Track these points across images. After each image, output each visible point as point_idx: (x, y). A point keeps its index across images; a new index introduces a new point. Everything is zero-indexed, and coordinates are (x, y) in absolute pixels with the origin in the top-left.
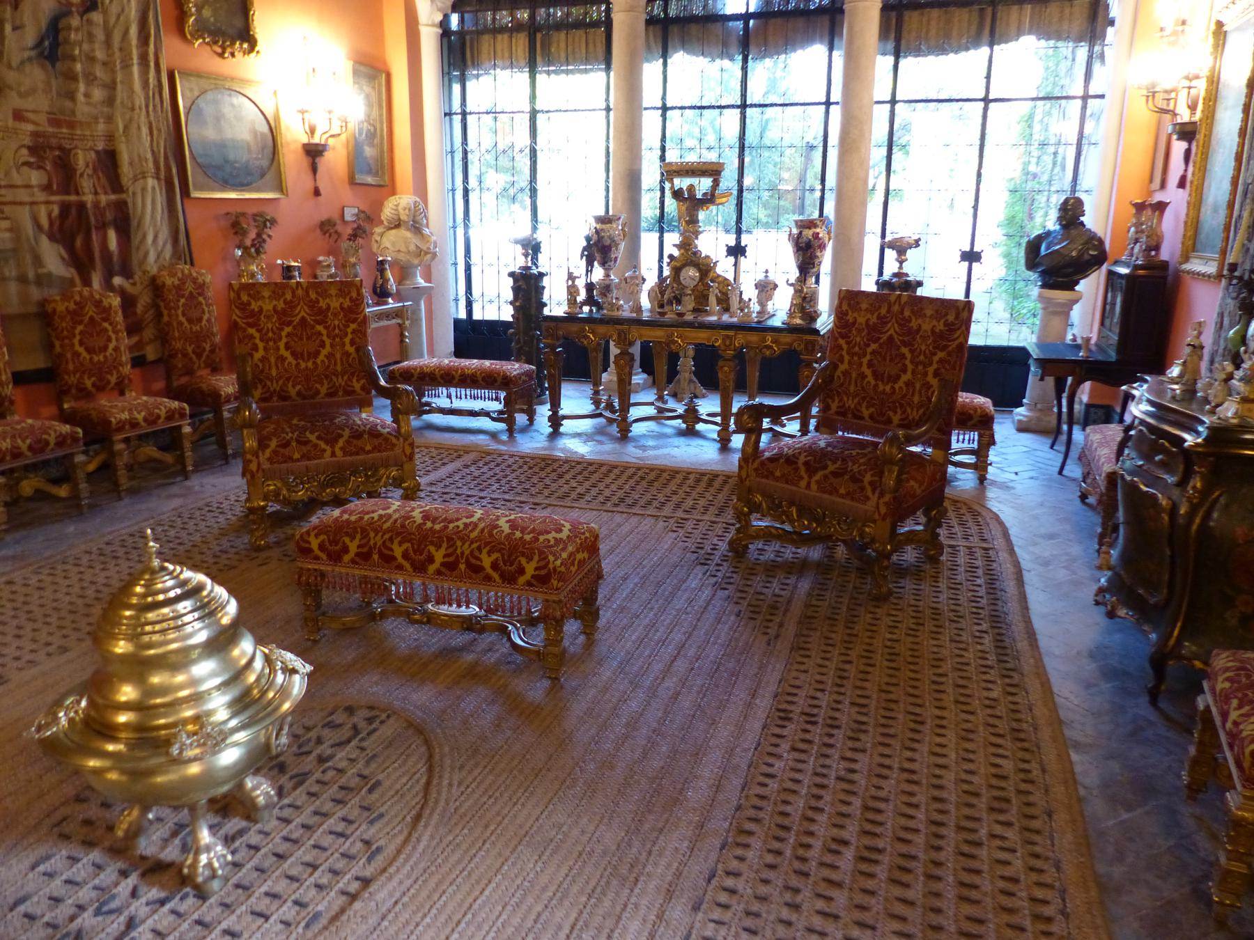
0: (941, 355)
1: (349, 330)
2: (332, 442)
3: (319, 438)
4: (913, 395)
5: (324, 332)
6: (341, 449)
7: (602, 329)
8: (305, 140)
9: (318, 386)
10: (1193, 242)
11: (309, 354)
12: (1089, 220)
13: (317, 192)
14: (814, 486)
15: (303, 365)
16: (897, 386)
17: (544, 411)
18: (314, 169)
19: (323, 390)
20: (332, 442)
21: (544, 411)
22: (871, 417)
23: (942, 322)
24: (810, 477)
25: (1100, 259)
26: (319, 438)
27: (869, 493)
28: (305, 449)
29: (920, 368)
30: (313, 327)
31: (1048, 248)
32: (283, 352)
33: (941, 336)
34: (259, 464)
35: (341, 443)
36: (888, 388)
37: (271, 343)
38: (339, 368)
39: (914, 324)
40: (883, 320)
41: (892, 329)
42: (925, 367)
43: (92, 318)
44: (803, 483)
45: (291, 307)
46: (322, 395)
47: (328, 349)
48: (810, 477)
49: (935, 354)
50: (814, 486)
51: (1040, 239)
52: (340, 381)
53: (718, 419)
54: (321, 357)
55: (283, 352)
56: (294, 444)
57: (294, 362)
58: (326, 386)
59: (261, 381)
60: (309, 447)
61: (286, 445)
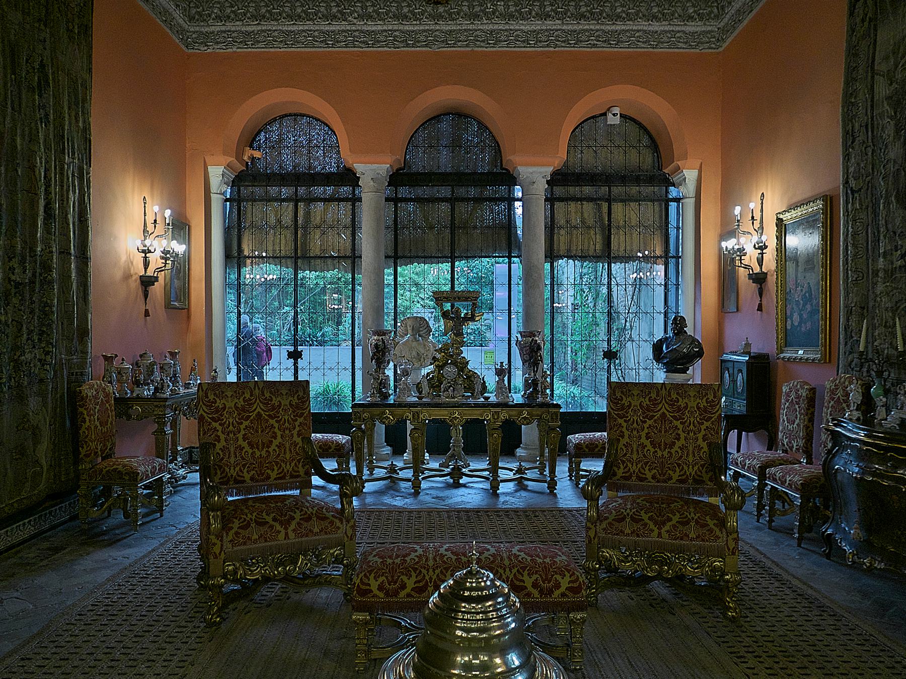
0: (707, 424)
1: (297, 423)
2: (286, 524)
3: (275, 520)
4: (285, 453)
5: (220, 428)
6: (294, 530)
7: (399, 411)
8: (142, 273)
9: (269, 471)
10: (788, 339)
11: (263, 444)
12: (689, 330)
13: (147, 313)
14: (291, 535)
15: (258, 454)
16: (271, 450)
17: (394, 485)
18: (146, 296)
19: (675, 477)
20: (286, 524)
21: (394, 485)
22: (654, 477)
23: (647, 399)
24: (286, 529)
25: (700, 354)
26: (650, 518)
27: (718, 533)
28: (636, 526)
29: (287, 432)
30: (267, 421)
31: (667, 348)
32: (241, 442)
33: (705, 410)
34: (222, 545)
35: (293, 525)
36: (264, 453)
37: (287, 432)
38: (635, 456)
39: (681, 403)
40: (654, 402)
41: (664, 408)
42: (638, 432)
43: (259, 414)
44: (282, 536)
45: (303, 402)
46: (618, 477)
47: (279, 439)
48: (286, 529)
49: (296, 420)
50: (291, 535)
51: (661, 342)
52: (634, 468)
53: (486, 473)
54: (273, 447)
55: (241, 442)
56: (693, 524)
57: (251, 451)
58: (276, 472)
59: (220, 467)
60: (266, 528)
61: (685, 523)
